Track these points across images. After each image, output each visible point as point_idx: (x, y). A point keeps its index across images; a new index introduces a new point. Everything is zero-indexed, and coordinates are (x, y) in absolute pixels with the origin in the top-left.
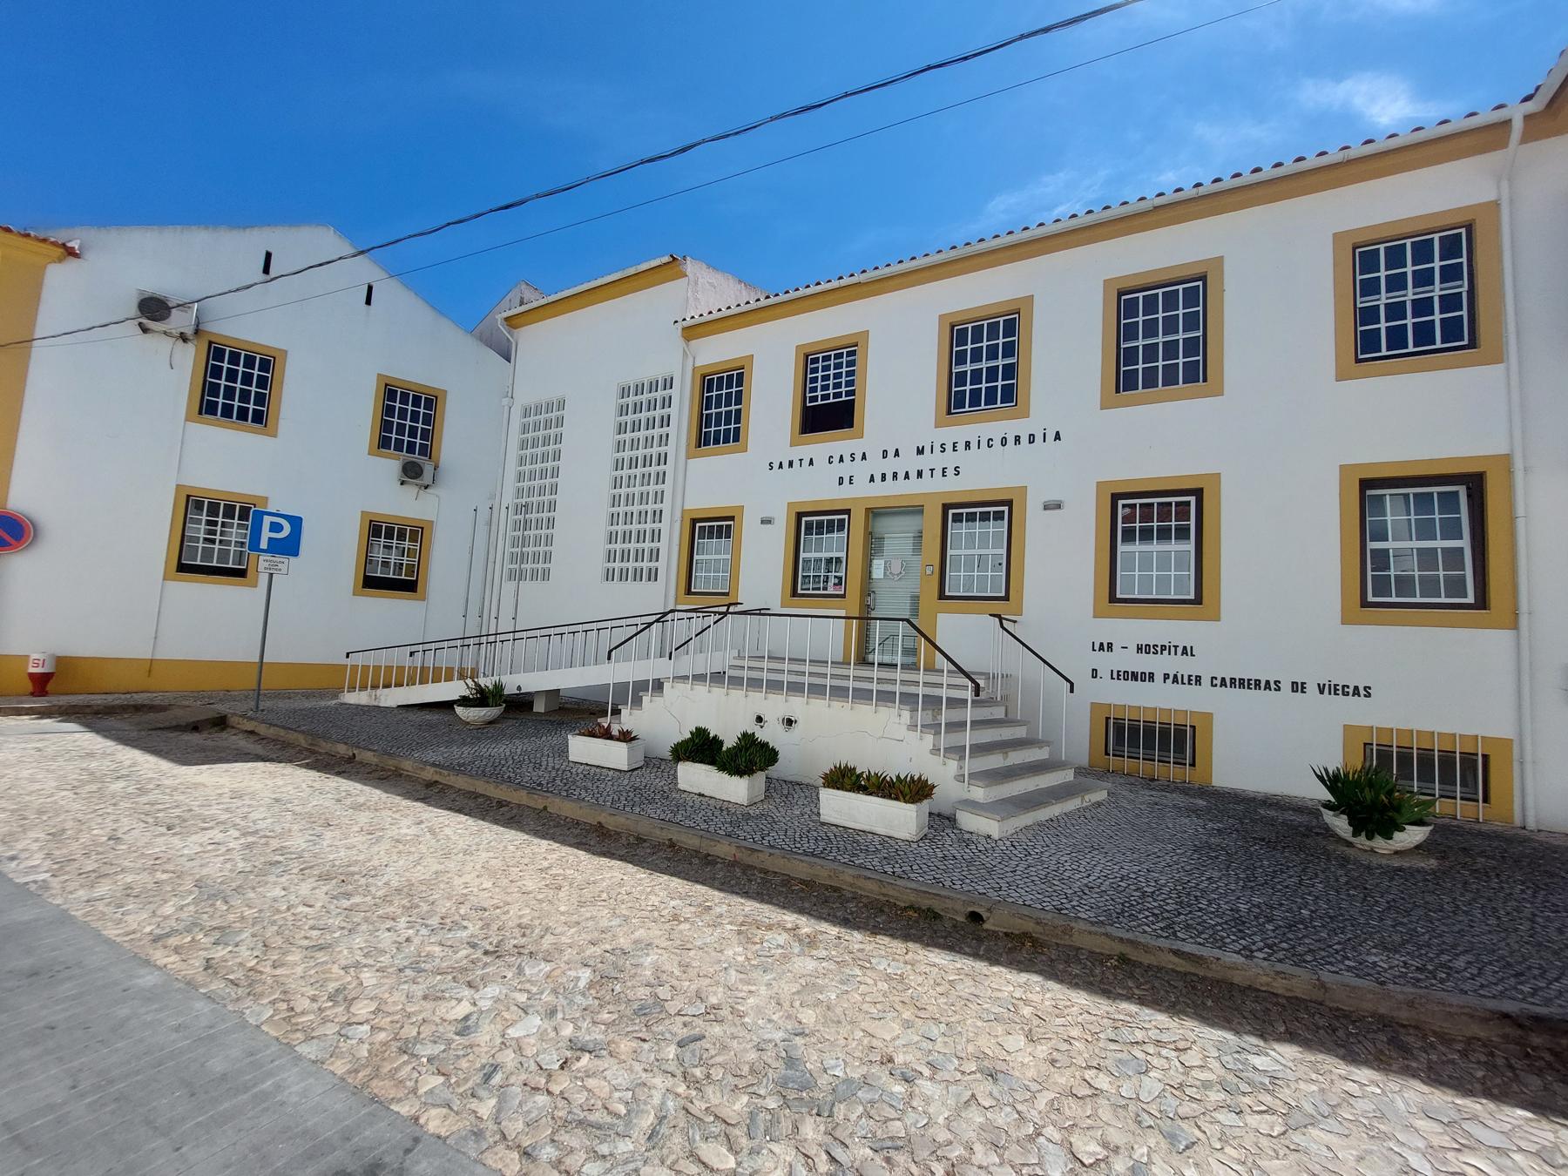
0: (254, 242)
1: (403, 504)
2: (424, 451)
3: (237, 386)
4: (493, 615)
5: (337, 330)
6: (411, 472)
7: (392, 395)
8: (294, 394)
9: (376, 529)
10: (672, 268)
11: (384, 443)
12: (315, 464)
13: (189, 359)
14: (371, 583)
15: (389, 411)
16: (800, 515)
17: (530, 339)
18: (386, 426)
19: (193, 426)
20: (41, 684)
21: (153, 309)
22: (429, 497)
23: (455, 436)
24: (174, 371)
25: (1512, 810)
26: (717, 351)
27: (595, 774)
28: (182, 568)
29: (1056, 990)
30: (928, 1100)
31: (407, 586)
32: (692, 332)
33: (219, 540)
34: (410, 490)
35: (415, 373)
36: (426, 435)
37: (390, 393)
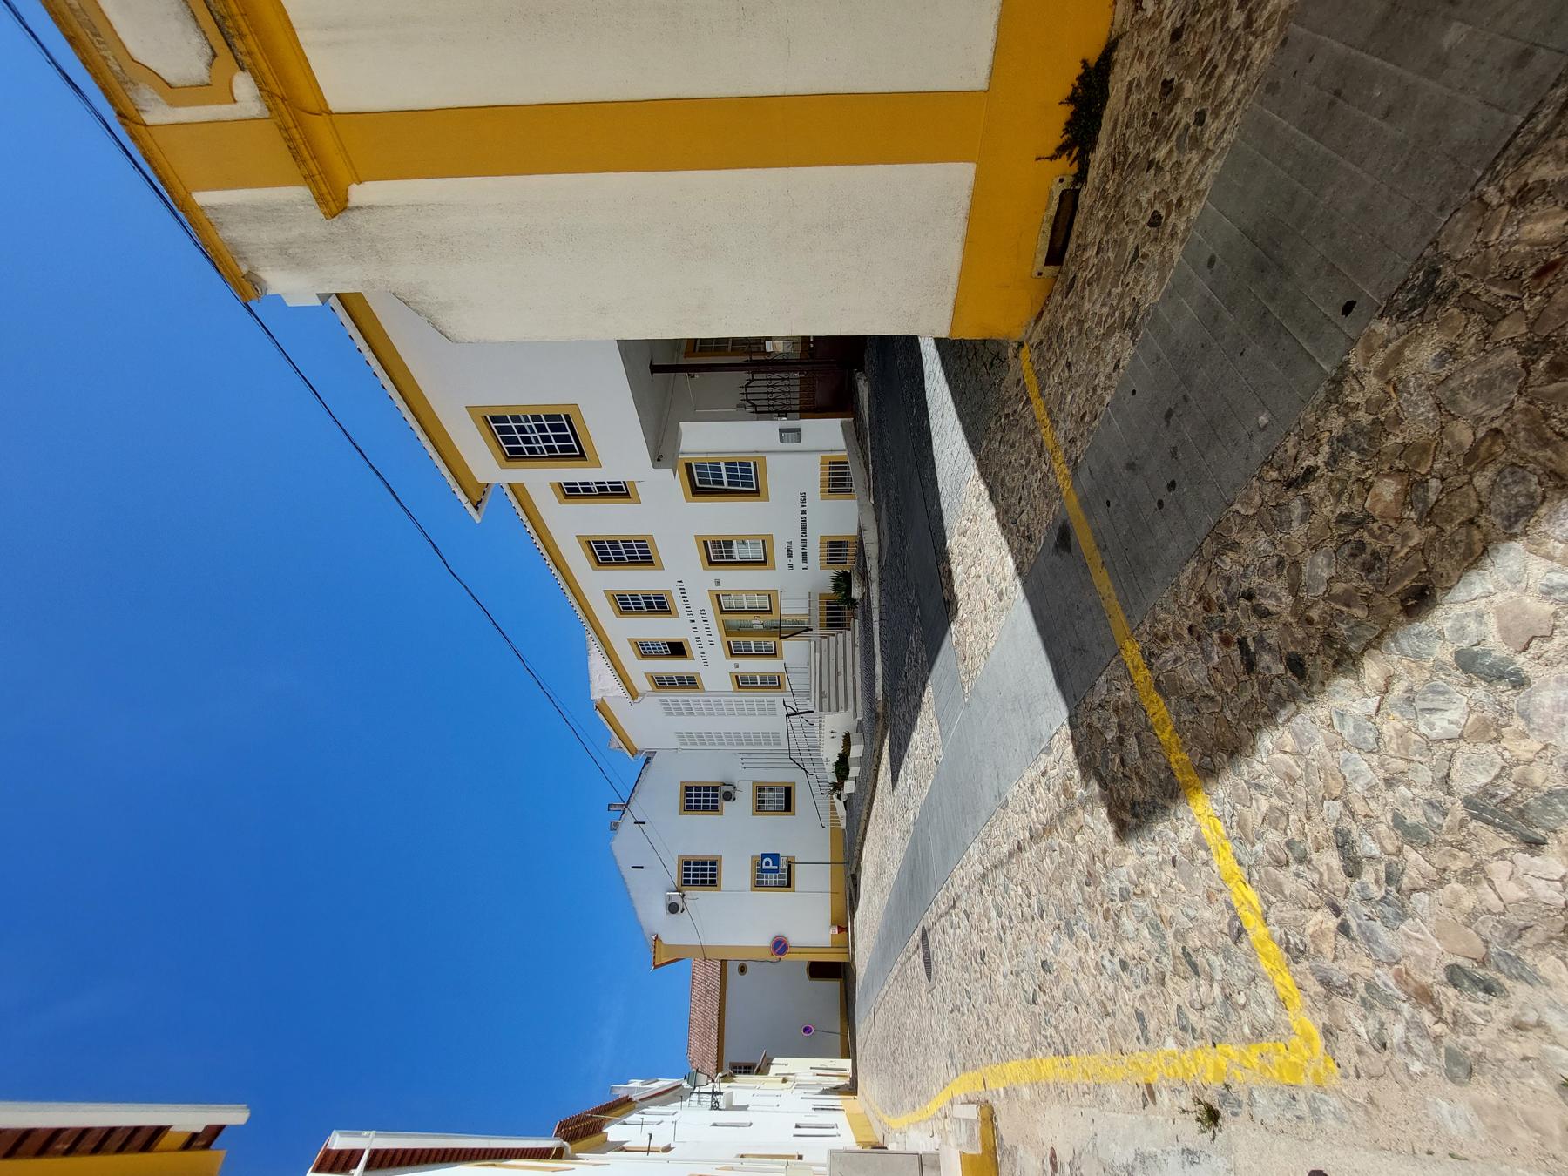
0: (632, 877)
1: (745, 798)
2: (715, 789)
4: (841, 678)
5: (660, 835)
6: (728, 797)
7: (689, 807)
9: (760, 807)
10: (601, 707)
11: (715, 809)
12: (735, 836)
13: (691, 893)
14: (788, 807)
15: (698, 808)
16: (711, 563)
17: (640, 742)
18: (706, 808)
19: (817, 458)
20: (843, 929)
21: (673, 908)
22: (740, 786)
24: (698, 897)
26: (642, 685)
28: (789, 885)
31: (788, 791)
32: (633, 694)
33: (774, 873)
35: (676, 798)
36: (706, 789)
37: (688, 808)
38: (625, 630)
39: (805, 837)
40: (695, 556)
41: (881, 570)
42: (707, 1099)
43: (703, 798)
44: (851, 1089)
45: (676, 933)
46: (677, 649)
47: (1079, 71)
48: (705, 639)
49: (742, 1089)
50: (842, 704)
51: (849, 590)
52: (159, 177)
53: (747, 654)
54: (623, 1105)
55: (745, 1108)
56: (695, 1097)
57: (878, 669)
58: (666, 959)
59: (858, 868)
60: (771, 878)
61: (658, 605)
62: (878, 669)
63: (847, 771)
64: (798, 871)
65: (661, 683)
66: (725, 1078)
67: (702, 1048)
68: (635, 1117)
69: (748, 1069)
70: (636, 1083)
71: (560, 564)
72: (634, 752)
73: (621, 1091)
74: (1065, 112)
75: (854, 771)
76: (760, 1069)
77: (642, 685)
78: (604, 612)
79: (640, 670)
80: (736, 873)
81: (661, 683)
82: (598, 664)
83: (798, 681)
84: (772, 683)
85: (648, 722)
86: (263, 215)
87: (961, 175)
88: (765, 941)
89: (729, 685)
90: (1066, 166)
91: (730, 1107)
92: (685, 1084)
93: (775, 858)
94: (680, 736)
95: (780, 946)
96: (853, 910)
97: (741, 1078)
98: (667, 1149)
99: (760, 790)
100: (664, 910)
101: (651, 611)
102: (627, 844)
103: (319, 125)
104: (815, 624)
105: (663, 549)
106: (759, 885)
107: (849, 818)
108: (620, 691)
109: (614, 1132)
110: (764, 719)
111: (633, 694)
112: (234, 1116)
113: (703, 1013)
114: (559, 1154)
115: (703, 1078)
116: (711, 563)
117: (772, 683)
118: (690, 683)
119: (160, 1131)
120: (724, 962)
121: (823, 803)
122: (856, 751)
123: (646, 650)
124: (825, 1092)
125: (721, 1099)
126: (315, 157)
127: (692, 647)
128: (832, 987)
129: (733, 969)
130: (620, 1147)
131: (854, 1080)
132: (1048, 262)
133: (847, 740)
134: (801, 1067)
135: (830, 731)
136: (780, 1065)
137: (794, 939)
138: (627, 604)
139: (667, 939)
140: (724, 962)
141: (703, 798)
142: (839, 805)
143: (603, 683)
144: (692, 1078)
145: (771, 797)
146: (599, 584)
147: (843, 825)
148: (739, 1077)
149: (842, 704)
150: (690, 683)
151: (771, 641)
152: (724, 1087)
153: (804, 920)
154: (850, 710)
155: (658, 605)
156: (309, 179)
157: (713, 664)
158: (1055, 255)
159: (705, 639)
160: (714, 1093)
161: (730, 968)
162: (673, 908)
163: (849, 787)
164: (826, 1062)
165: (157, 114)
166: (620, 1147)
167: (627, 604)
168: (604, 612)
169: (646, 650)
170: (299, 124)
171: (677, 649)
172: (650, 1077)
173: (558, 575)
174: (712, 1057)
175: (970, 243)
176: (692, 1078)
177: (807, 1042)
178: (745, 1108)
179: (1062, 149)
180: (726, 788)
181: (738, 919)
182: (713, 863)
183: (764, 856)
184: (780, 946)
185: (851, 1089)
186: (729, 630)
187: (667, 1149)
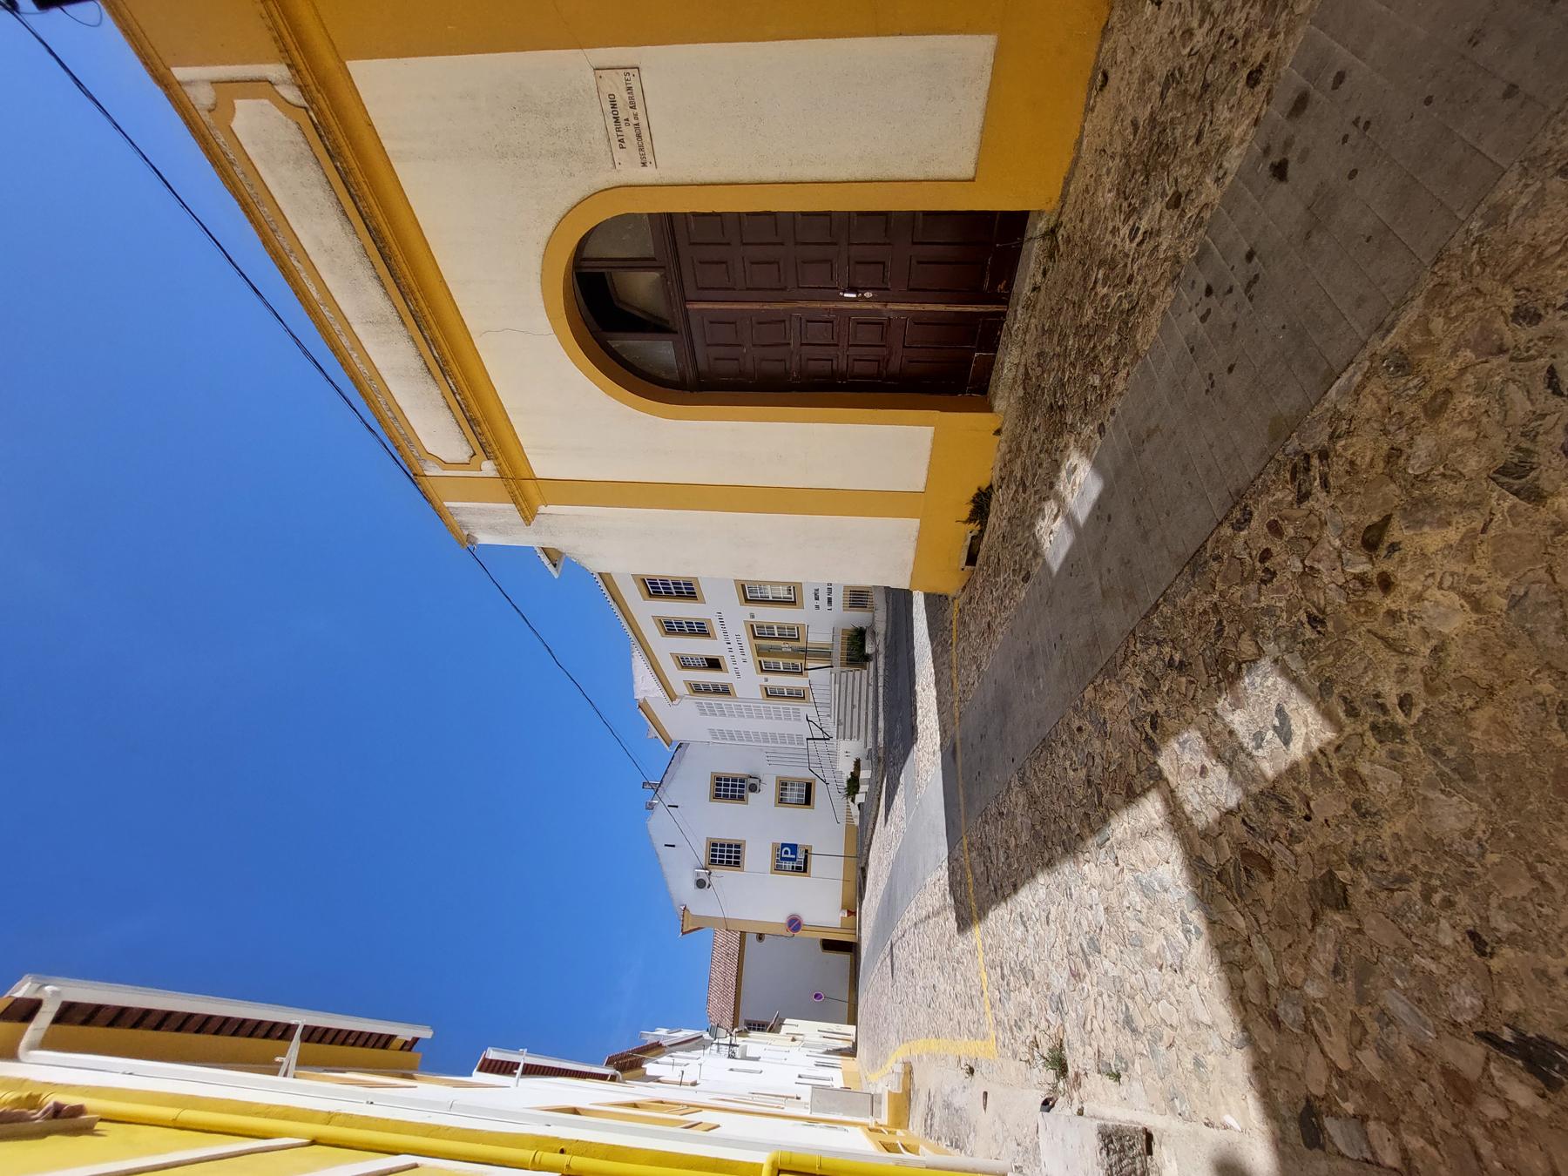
0: (665, 853)
1: (769, 791)
3: (726, 855)
5: (687, 820)
6: (753, 788)
8: (727, 834)
11: (741, 798)
12: (759, 824)
13: (717, 871)
14: (808, 801)
15: (726, 796)
16: (747, 600)
17: (676, 735)
18: (733, 797)
20: (851, 913)
21: (701, 884)
23: (733, 767)
25: (919, 321)
27: (1095, 488)
29: (1199, 951)
30: (1473, 657)
31: (809, 786)
32: (672, 697)
33: (793, 859)
34: (762, 787)
35: (706, 787)
37: (717, 796)
38: (667, 648)
39: (821, 828)
40: (734, 596)
41: (886, 647)
42: (725, 1050)
43: (730, 789)
44: (852, 1052)
45: (702, 905)
46: (714, 664)
47: (975, 491)
48: (739, 658)
49: (755, 1043)
50: (855, 733)
51: (863, 647)
52: (354, 378)
53: (777, 671)
54: (656, 1048)
55: (757, 1059)
56: (715, 1047)
57: (881, 724)
58: (691, 927)
59: (867, 863)
60: (789, 865)
61: (700, 630)
62: (881, 724)
63: (858, 787)
64: (814, 862)
65: (697, 689)
66: (740, 1033)
67: (719, 1004)
68: (665, 1059)
69: (760, 1027)
70: (662, 1032)
71: (616, 598)
72: (669, 743)
73: (650, 1038)
74: (971, 507)
75: (864, 788)
76: (774, 1028)
77: (680, 688)
78: (652, 633)
79: (679, 679)
80: (758, 856)
81: (697, 689)
82: (640, 665)
83: (820, 695)
84: (798, 696)
85: (684, 719)
86: (481, 512)
87: (915, 523)
88: (782, 919)
89: (759, 695)
90: (974, 528)
91: (745, 1058)
92: (706, 1036)
93: (794, 848)
94: (712, 731)
95: (795, 924)
96: (862, 898)
97: (755, 1035)
98: (694, 1084)
99: (783, 785)
100: (692, 885)
101: (692, 633)
102: (660, 825)
103: (529, 485)
104: (838, 652)
105: (705, 589)
106: (778, 869)
107: (861, 817)
108: (661, 693)
109: (651, 1068)
110: (792, 723)
111: (672, 697)
112: (425, 1033)
113: (721, 973)
114: (613, 1078)
115: (722, 1032)
116: (747, 600)
117: (798, 696)
118: (725, 691)
119: (392, 1037)
120: (743, 934)
121: (840, 801)
122: (865, 774)
123: (684, 663)
124: (828, 1052)
125: (738, 1051)
126: (525, 500)
127: (727, 662)
128: (845, 958)
129: (751, 940)
130: (656, 1079)
131: (855, 1045)
132: (968, 563)
133: (857, 764)
134: (810, 1029)
135: (846, 753)
136: (791, 1026)
137: (807, 918)
138: (671, 628)
139: (695, 910)
140: (743, 934)
141: (730, 789)
142: (855, 811)
143: (645, 685)
144: (713, 1032)
145: (793, 794)
146: (648, 612)
147: (857, 822)
148: (753, 1034)
149: (855, 733)
150: (725, 691)
151: (798, 662)
152: (739, 1040)
153: (817, 901)
154: (862, 739)
155: (700, 630)
156: (515, 502)
157: (744, 675)
158: (972, 559)
159: (739, 658)
160: (731, 1045)
161: (746, 939)
162: (701, 884)
163: (860, 798)
164: (833, 1027)
165: (432, 470)
166: (656, 1079)
167: (671, 628)
168: (652, 633)
169: (684, 663)
170: (519, 487)
171: (714, 664)
172: (674, 1026)
173: (614, 606)
174: (729, 1014)
175: (918, 551)
176: (713, 1032)
177: (817, 1007)
178: (757, 1059)
179: (970, 520)
180: (752, 781)
181: (758, 897)
182: (738, 846)
183: (784, 845)
184: (795, 924)
185: (852, 1052)
186: (760, 651)
187: (694, 1084)
